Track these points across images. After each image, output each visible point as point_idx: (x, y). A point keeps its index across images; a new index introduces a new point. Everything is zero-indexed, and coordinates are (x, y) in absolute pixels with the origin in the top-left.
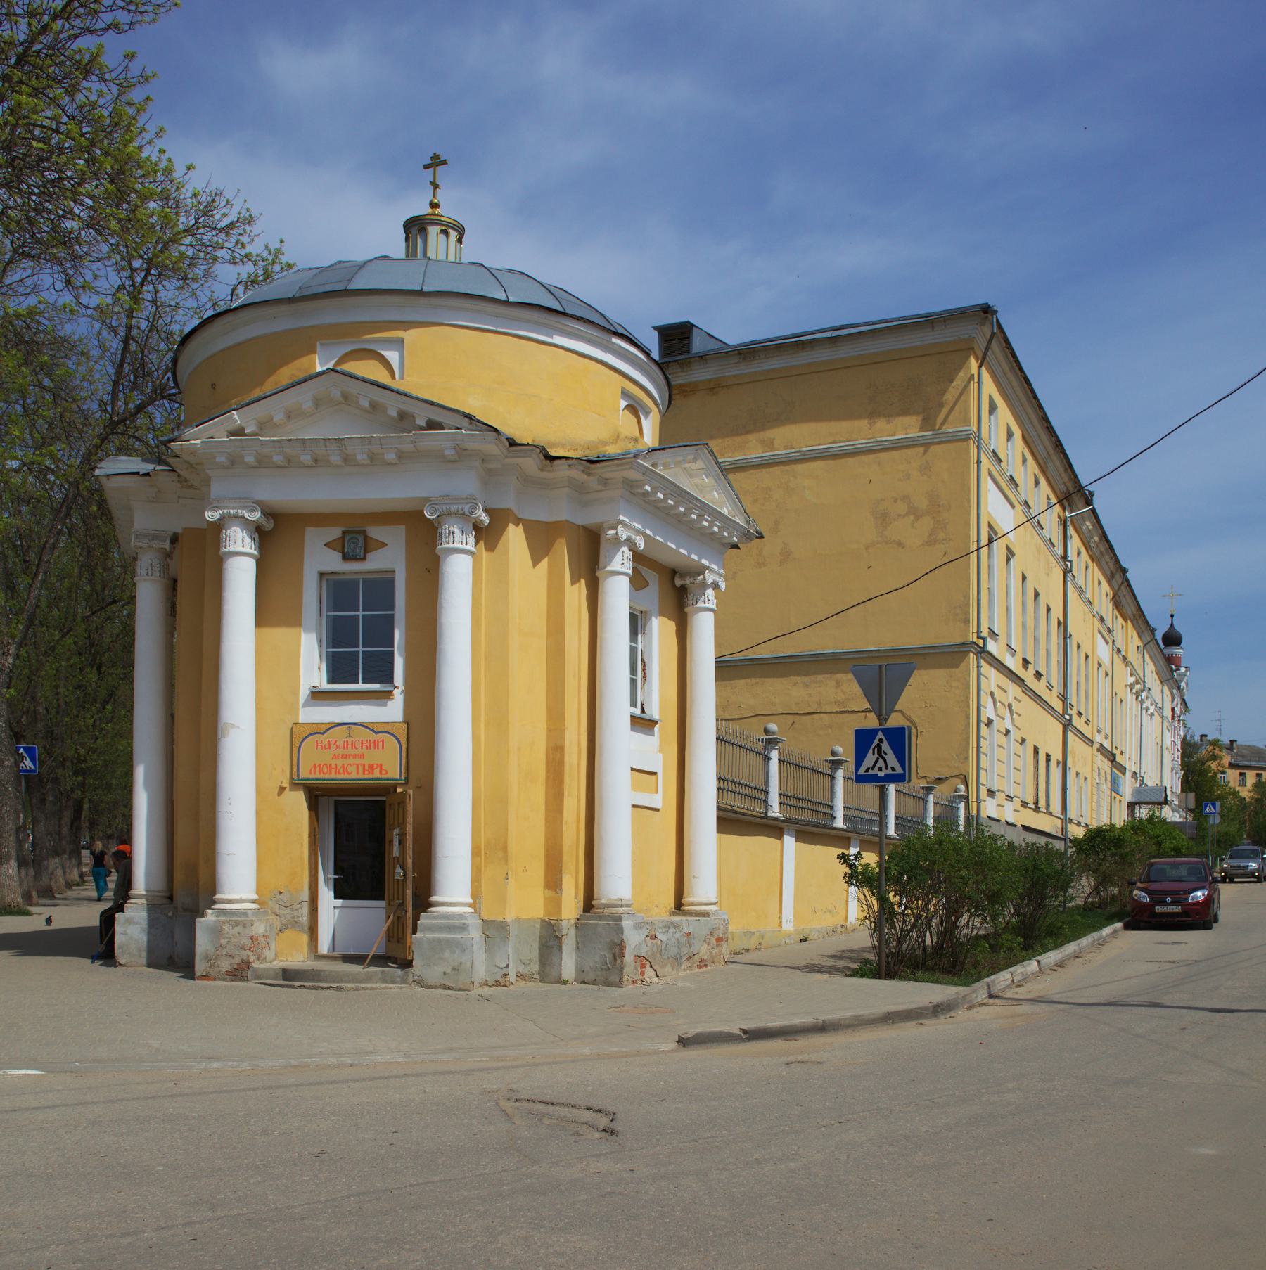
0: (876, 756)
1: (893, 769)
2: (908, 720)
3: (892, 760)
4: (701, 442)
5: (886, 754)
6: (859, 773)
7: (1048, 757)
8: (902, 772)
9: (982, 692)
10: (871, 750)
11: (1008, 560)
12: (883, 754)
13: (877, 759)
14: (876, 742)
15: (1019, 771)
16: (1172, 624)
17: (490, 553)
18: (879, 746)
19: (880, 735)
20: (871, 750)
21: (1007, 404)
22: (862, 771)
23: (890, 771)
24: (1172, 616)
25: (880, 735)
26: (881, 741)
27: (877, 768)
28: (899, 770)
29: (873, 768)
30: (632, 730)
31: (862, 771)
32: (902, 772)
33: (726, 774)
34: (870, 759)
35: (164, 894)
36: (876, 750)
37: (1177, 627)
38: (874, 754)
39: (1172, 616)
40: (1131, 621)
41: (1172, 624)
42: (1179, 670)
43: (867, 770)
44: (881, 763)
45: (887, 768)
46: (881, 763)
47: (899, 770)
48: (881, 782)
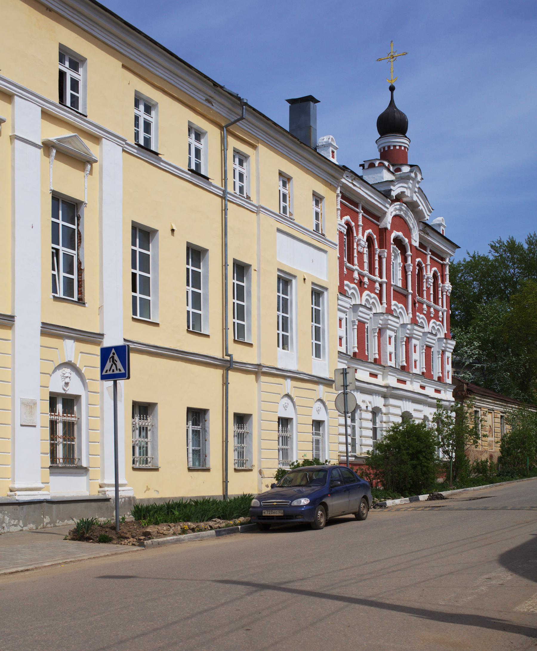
0: (111, 363)
1: (120, 370)
4: (504, 399)
5: (116, 362)
6: (103, 374)
8: (124, 372)
9: (345, 604)
12: (115, 362)
13: (112, 365)
14: (111, 355)
15: (80, 75)
16: (392, 101)
18: (113, 357)
19: (113, 351)
20: (109, 360)
21: (94, 345)
23: (118, 372)
24: (392, 89)
25: (113, 351)
26: (114, 354)
27: (111, 370)
28: (123, 371)
29: (110, 371)
30: (41, 336)
31: (104, 373)
32: (124, 372)
36: (111, 359)
37: (399, 105)
38: (110, 362)
39: (392, 89)
41: (392, 101)
42: (399, 170)
44: (114, 367)
45: (117, 370)
46: (114, 367)
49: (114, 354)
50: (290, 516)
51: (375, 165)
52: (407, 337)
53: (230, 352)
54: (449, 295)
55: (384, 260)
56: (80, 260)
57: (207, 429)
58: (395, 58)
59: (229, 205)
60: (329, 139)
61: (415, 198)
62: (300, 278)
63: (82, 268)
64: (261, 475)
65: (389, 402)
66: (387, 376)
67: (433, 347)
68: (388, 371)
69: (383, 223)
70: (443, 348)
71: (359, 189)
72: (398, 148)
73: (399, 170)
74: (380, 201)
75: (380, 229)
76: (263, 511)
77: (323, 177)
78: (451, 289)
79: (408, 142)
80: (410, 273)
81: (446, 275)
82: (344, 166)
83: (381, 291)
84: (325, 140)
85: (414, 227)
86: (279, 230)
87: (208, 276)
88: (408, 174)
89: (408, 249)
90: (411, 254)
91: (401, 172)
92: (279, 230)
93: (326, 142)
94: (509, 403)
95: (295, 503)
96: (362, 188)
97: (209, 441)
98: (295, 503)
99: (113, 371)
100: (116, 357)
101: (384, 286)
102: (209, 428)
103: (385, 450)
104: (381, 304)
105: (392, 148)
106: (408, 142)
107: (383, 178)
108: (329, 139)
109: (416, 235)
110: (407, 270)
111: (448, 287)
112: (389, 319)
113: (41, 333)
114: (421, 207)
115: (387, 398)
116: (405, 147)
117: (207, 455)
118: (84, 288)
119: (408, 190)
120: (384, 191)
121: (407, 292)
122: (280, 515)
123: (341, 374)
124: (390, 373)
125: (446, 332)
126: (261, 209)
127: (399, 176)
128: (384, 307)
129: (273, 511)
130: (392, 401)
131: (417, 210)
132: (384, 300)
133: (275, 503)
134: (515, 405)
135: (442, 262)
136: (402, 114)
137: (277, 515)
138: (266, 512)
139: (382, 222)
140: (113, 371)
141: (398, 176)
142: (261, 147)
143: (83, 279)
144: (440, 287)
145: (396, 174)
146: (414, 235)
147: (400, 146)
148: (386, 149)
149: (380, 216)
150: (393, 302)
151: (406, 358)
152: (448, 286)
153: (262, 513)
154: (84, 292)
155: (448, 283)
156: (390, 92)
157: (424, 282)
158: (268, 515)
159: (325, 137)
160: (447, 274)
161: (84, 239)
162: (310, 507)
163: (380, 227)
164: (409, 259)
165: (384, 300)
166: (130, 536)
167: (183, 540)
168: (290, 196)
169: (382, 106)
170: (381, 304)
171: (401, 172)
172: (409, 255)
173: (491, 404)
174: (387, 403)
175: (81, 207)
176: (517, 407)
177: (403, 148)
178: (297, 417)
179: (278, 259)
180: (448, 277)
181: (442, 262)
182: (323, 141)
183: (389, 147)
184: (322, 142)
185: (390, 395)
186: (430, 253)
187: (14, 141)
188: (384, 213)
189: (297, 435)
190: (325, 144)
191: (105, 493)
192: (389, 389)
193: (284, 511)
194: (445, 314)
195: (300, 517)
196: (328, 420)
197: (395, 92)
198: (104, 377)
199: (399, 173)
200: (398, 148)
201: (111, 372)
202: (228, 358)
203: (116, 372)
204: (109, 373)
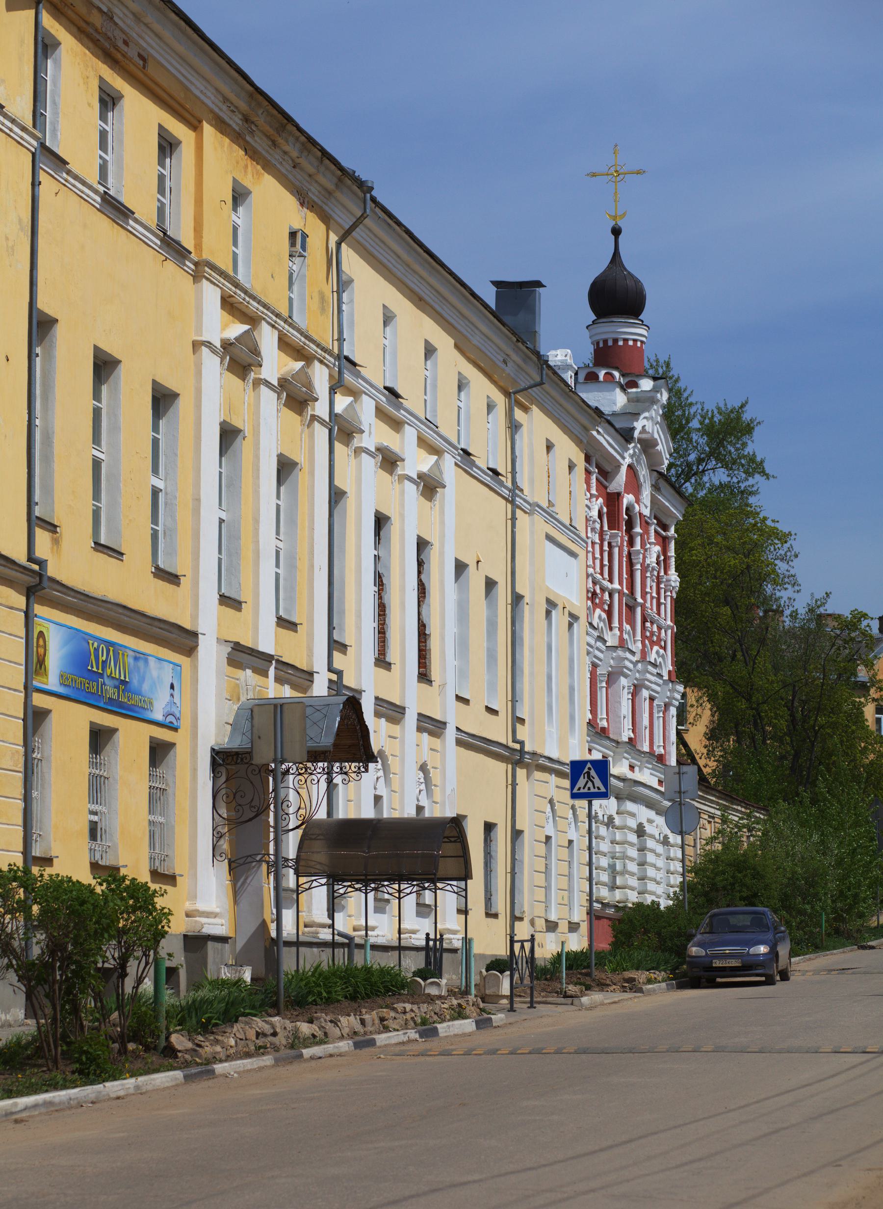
0: (586, 779)
1: (599, 788)
2: (514, 785)
3: (598, 782)
7: (491, 915)
10: (582, 776)
11: (570, 625)
14: (586, 770)
16: (616, 254)
17: (278, 685)
18: (588, 773)
19: (589, 765)
22: (575, 791)
23: (596, 790)
24: (616, 232)
25: (589, 765)
26: (589, 769)
27: (587, 788)
28: (603, 790)
29: (584, 788)
31: (575, 791)
33: (658, 740)
34: (581, 782)
35: (326, 868)
39: (616, 232)
40: (222, 126)
41: (616, 254)
42: (635, 385)
43: (579, 789)
44: (590, 784)
45: (594, 788)
47: (603, 790)
48: (590, 796)
49: (589, 769)
50: (750, 967)
51: (597, 377)
52: (635, 685)
53: (519, 737)
54: (675, 597)
55: (616, 550)
56: (422, 622)
57: (493, 854)
58: (621, 177)
59: (518, 512)
60: (566, 356)
61: (656, 436)
62: (560, 607)
63: (427, 632)
64: (533, 927)
65: (626, 806)
66: (620, 760)
67: (656, 697)
68: (624, 750)
69: (615, 485)
70: (667, 700)
71: (602, 438)
72: (631, 343)
73: (635, 385)
74: (616, 447)
75: (608, 494)
76: (714, 961)
77: (576, 433)
78: (678, 584)
79: (644, 332)
80: (638, 566)
81: (670, 557)
82: (597, 408)
83: (611, 606)
84: (559, 358)
85: (645, 482)
86: (549, 538)
87: (497, 622)
88: (649, 395)
89: (636, 523)
90: (641, 531)
91: (639, 390)
92: (549, 538)
93: (561, 361)
94: (735, 801)
95: (753, 950)
96: (606, 436)
97: (496, 872)
98: (753, 950)
99: (589, 789)
100: (593, 773)
101: (616, 596)
102: (497, 852)
103: (13, 908)
104: (611, 629)
105: (621, 343)
106: (644, 332)
107: (615, 404)
108: (566, 356)
109: (647, 495)
110: (634, 561)
111: (675, 582)
112: (627, 659)
113: (417, 728)
114: (659, 447)
115: (622, 799)
116: (642, 342)
117: (493, 893)
118: (430, 661)
119: (650, 421)
120: (621, 428)
121: (633, 601)
122: (737, 965)
123: (675, 774)
124: (626, 755)
125: (671, 668)
126: (537, 508)
127: (634, 396)
128: (614, 635)
129: (728, 961)
130: (630, 806)
131: (651, 451)
132: (616, 624)
133: (728, 952)
134: (742, 807)
135: (664, 533)
136: (637, 282)
137: (731, 965)
138: (718, 962)
139: (612, 481)
140: (589, 789)
141: (631, 396)
142: (535, 409)
143: (428, 648)
144: (663, 582)
145: (629, 390)
146: (644, 496)
147: (635, 341)
148: (610, 343)
149: (610, 470)
150: (624, 623)
151: (633, 723)
152: (674, 577)
153: (711, 962)
154: (430, 665)
155: (674, 574)
156: (613, 237)
157: (647, 577)
158: (721, 965)
159: (559, 352)
160: (672, 556)
161: (429, 593)
162: (771, 956)
163: (608, 491)
164: (638, 540)
165: (616, 624)
166: (611, 983)
167: (654, 990)
168: (550, 474)
169: (599, 265)
170: (611, 629)
171: (639, 390)
172: (638, 533)
173: (713, 805)
174: (622, 808)
175: (425, 548)
176: (743, 810)
177: (639, 344)
178: (556, 835)
179: (547, 584)
180: (672, 562)
181: (664, 533)
182: (557, 359)
183: (616, 341)
184: (555, 361)
185: (628, 795)
186: (655, 521)
187: (403, 481)
188: (616, 467)
189: (557, 864)
190: (560, 364)
191: (451, 942)
192: (627, 784)
193: (742, 961)
194: (669, 632)
195: (760, 968)
196: (578, 840)
197: (621, 238)
198: (574, 796)
199: (634, 390)
200: (631, 343)
201: (586, 790)
202: (517, 746)
203: (592, 790)
204: (582, 791)
